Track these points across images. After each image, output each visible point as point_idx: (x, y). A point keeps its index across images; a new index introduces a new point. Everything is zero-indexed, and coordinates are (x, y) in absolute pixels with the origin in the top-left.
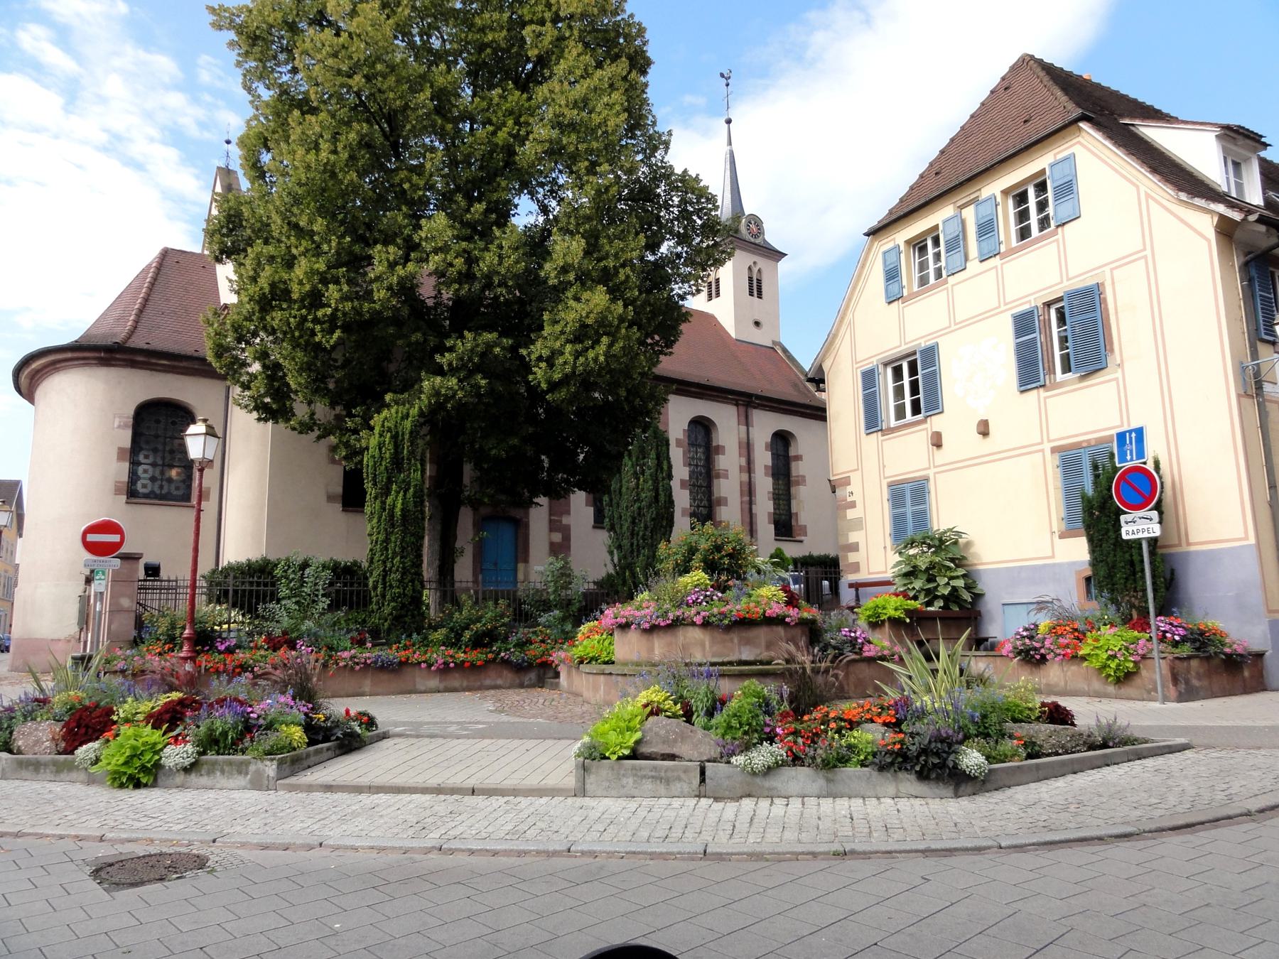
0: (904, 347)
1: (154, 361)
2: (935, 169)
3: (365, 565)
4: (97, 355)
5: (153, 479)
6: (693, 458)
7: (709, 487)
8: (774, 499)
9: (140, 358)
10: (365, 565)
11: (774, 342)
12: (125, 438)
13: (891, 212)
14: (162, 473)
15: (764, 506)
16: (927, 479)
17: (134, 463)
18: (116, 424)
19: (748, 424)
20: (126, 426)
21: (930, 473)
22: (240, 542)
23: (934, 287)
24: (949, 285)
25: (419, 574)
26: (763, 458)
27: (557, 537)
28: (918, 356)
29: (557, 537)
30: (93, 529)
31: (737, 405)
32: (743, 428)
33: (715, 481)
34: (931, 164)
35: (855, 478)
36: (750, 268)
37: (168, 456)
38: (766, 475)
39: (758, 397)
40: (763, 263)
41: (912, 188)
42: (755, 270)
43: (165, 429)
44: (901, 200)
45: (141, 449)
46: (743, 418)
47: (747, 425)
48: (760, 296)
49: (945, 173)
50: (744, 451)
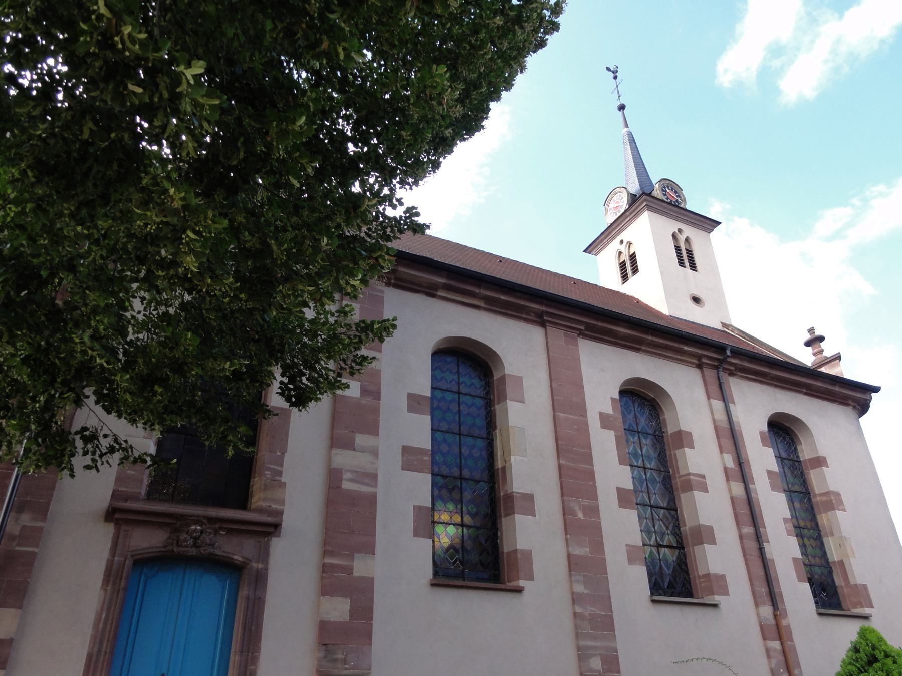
6: (635, 455)
7: (673, 508)
19: (725, 397)
26: (763, 459)
27: (338, 609)
29: (338, 609)
31: (700, 366)
32: (718, 404)
33: (683, 498)
42: (682, 238)
46: (714, 388)
48: (693, 267)
50: (728, 443)
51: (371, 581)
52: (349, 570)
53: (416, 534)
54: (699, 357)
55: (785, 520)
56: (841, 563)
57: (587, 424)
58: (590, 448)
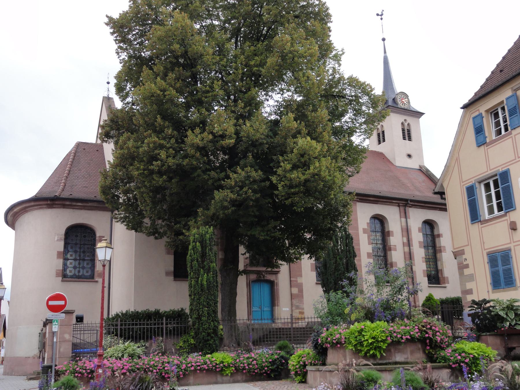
0: (489, 172)
1: (74, 204)
2: (500, 69)
3: (188, 311)
4: (46, 203)
5: (75, 268)
8: (426, 262)
9: (68, 203)
10: (188, 311)
11: (420, 166)
12: (60, 246)
13: (476, 94)
14: (79, 264)
15: (420, 267)
16: (510, 250)
17: (66, 259)
18: (56, 239)
20: (61, 239)
21: (512, 246)
22: (121, 302)
23: (505, 136)
24: (513, 135)
25: (216, 316)
26: (417, 237)
28: (498, 177)
30: (52, 298)
31: (399, 206)
32: (403, 220)
33: (389, 252)
34: (498, 65)
35: (467, 250)
36: (402, 124)
37: (82, 255)
38: (420, 247)
39: (412, 201)
40: (410, 120)
41: (487, 80)
42: (406, 124)
43: (80, 240)
44: (482, 87)
45: (68, 251)
46: (403, 214)
47: (406, 217)
48: (410, 139)
49: (506, 70)
50: (405, 233)
51: (302, 283)
52: (297, 281)
53: (312, 271)
54: (399, 203)
55: (423, 258)
56: (441, 270)
57: (358, 233)
58: (359, 241)
